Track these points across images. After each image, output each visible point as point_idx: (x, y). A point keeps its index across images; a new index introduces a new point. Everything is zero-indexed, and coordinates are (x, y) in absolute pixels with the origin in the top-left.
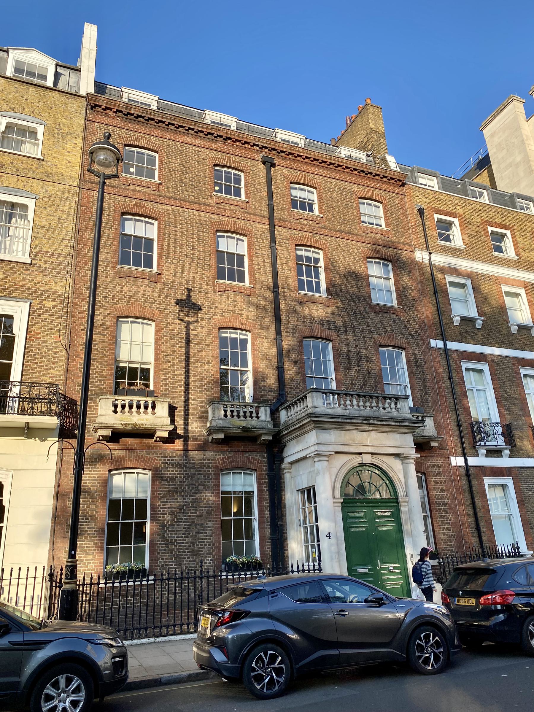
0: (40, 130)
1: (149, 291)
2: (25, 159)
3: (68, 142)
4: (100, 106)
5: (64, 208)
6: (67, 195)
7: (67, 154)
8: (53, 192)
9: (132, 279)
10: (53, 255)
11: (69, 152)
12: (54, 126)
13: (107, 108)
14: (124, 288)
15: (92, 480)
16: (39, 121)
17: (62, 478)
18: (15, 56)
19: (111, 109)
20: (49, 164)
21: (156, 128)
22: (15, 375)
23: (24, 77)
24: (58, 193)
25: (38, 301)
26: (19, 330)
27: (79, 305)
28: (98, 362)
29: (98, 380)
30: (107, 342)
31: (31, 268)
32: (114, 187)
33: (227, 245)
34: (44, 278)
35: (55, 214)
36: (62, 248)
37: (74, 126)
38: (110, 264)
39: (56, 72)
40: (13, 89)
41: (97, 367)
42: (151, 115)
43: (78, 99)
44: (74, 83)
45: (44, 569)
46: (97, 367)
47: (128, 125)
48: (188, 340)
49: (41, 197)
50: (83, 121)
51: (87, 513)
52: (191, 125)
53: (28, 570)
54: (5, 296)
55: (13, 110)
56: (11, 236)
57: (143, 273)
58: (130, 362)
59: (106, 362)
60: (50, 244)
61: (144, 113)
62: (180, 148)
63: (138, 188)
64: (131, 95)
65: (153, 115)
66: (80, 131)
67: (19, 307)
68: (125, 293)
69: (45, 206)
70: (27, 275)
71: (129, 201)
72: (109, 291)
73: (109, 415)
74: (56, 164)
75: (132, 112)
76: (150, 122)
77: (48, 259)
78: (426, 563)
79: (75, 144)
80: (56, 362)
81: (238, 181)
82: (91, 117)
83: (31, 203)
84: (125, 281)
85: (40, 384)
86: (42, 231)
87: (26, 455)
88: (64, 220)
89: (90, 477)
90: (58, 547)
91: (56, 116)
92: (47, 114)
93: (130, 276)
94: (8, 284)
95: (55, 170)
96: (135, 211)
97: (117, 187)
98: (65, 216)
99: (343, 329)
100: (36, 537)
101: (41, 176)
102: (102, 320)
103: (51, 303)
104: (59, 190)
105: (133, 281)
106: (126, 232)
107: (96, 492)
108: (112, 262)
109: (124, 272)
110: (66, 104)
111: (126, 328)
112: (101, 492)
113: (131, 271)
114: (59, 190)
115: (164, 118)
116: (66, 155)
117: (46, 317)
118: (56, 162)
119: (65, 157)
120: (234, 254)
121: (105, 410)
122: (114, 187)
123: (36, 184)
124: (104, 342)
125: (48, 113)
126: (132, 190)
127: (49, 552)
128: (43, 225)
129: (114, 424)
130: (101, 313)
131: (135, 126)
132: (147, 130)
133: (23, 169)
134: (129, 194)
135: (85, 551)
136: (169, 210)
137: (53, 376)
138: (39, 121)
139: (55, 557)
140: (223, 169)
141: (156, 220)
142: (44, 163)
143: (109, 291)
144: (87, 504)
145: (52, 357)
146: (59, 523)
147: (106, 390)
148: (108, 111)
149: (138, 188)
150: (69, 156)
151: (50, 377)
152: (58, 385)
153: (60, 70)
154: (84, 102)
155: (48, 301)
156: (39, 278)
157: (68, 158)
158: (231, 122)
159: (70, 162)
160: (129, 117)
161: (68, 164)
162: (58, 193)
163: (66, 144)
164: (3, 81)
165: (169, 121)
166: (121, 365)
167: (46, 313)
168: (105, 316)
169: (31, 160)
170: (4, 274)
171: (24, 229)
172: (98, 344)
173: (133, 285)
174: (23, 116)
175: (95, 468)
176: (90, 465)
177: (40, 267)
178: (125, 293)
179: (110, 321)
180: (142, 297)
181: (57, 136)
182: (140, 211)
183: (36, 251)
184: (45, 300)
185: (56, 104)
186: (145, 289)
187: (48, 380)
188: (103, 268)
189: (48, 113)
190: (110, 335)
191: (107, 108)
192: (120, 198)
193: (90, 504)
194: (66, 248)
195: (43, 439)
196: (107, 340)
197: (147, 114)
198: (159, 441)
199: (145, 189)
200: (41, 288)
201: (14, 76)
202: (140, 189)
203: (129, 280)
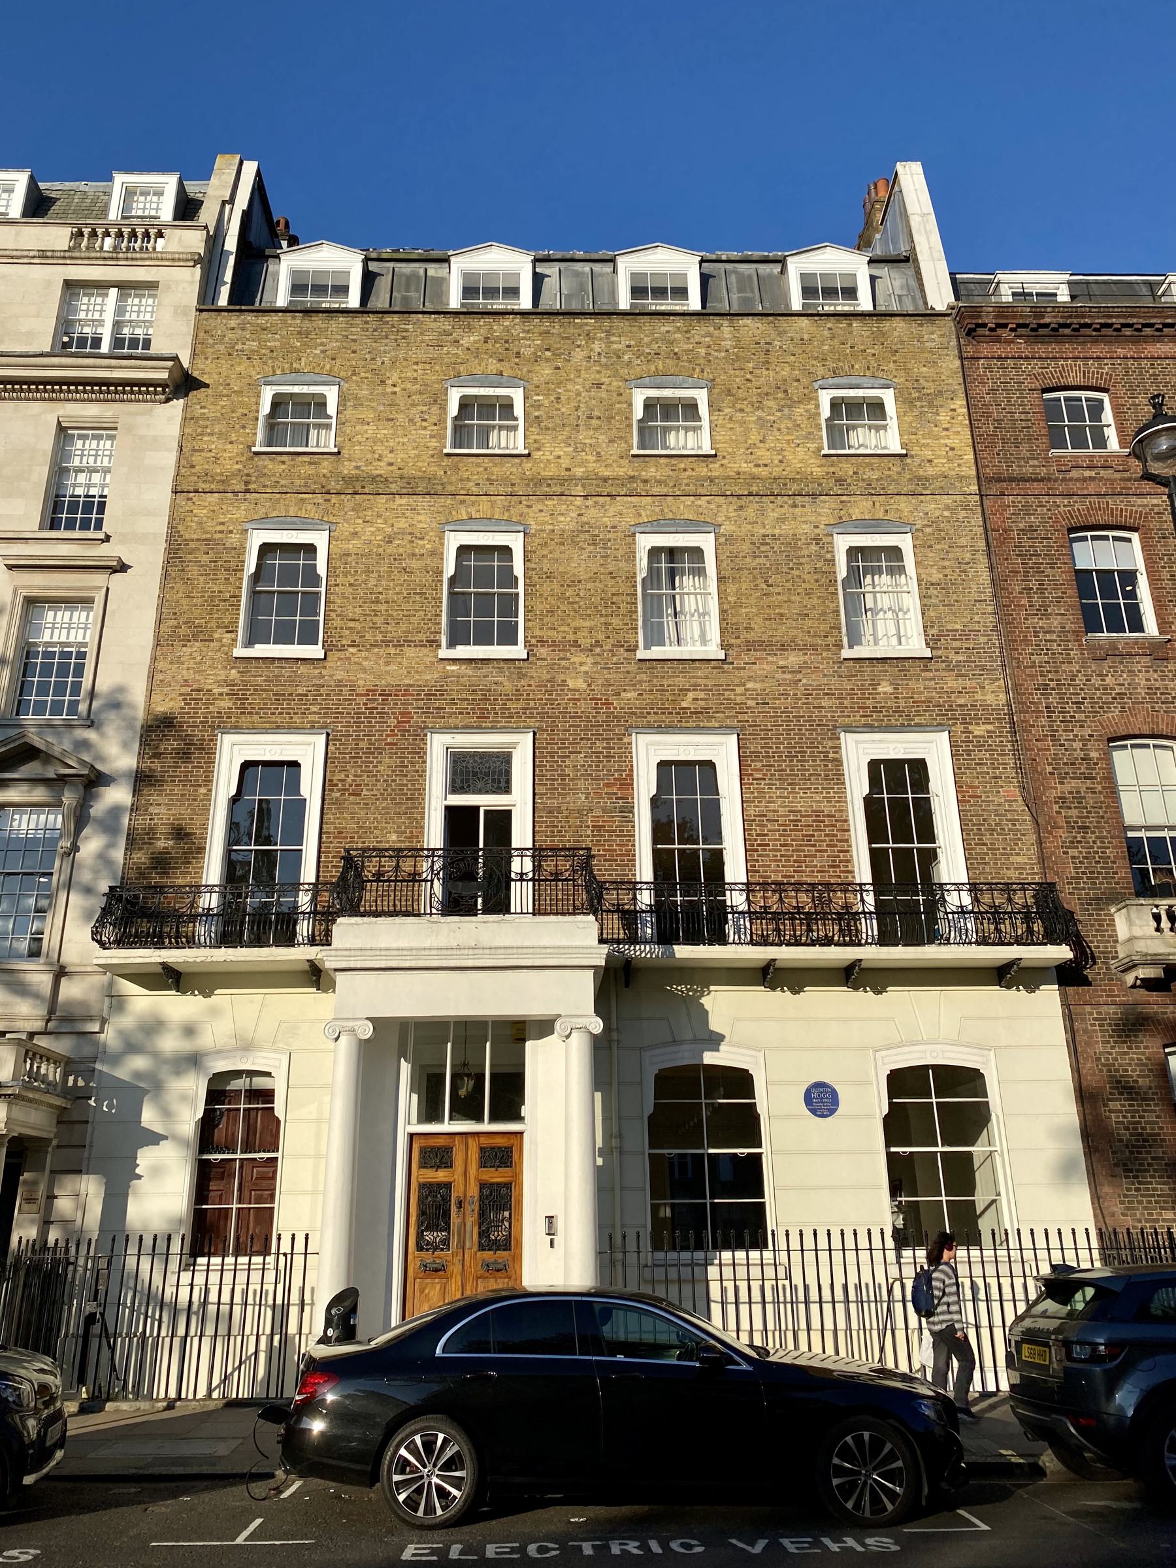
0: (888, 398)
1: (1156, 680)
2: (875, 460)
3: (940, 410)
4: (984, 325)
5: (963, 541)
6: (962, 514)
7: (945, 433)
8: (937, 513)
9: (1118, 659)
10: (965, 635)
11: (947, 429)
12: (909, 385)
13: (999, 326)
14: (1108, 679)
15: (1136, 1065)
16: (882, 381)
17: (1081, 1060)
18: (629, 265)
19: (1005, 326)
20: (917, 460)
21: (1095, 340)
22: (735, 870)
23: (309, 300)
24: (946, 514)
26: (311, 786)
27: (1033, 726)
28: (1093, 832)
29: (1102, 868)
30: (1100, 793)
31: (932, 666)
32: (1042, 480)
33: (1093, 555)
34: (960, 681)
35: (951, 555)
36: (976, 618)
37: (943, 377)
38: (1070, 637)
39: (535, 274)
40: (826, 333)
41: (1094, 842)
42: (1084, 317)
43: (939, 321)
44: (902, 288)
45: (183, 1239)
46: (1094, 842)
47: (1041, 349)
49: (918, 527)
50: (958, 363)
51: (1142, 1128)
52: (1168, 317)
53: (113, 1240)
54: (903, 725)
55: (834, 373)
56: (871, 609)
57: (1136, 643)
58: (1148, 828)
59: (1109, 832)
60: (954, 614)
61: (1070, 317)
62: (1151, 371)
63: (1087, 473)
64: (1010, 283)
65: (1090, 316)
66: (956, 383)
67: (309, 744)
68: (1112, 689)
69: (929, 543)
70: (930, 680)
71: (1078, 505)
72: (1082, 689)
73: (1152, 938)
74: (929, 458)
75: (1047, 320)
76: (1083, 331)
77: (957, 644)
78: (941, 1267)
79: (954, 410)
80: (1019, 839)
81: (1096, 409)
82: (970, 350)
83: (905, 542)
84: (1105, 665)
85: (798, 886)
86: (935, 592)
87: (1008, 1018)
88: (968, 563)
89: (1132, 1059)
90: (1107, 1194)
91: (909, 366)
92: (892, 365)
93: (1113, 652)
94: (902, 703)
95: (930, 471)
96: (1092, 521)
97: (1049, 480)
98: (968, 556)
100: (1065, 1171)
101: (912, 487)
102: (1081, 750)
103: (984, 727)
104: (947, 508)
105: (1122, 663)
106: (1080, 566)
107: (1150, 1088)
108: (1074, 632)
109: (1100, 647)
110: (920, 338)
111: (1122, 759)
112: (1159, 1087)
113: (1113, 644)
114: (947, 508)
115: (1112, 317)
116: (942, 438)
117: (981, 755)
118: (928, 453)
119: (942, 441)
120: (1091, 571)
121: (1140, 927)
122: (1042, 480)
123: (904, 505)
124: (1095, 793)
125: (895, 362)
126: (1077, 480)
127: (1093, 1203)
128: (934, 581)
129: (1169, 954)
130: (1076, 736)
131: (1053, 348)
132: (1079, 350)
133: (877, 480)
134: (1075, 487)
135: (1156, 1202)
136: (1158, 505)
137: (1020, 868)
138: (882, 381)
139: (1105, 1213)
140: (1062, 395)
141: (1135, 529)
142: (909, 461)
143: (1082, 689)
144: (1138, 1111)
145: (1010, 830)
146: (1097, 1150)
147: (1122, 888)
148: (1000, 331)
149: (1087, 473)
150: (948, 437)
151: (1016, 869)
153: (373, 267)
154: (949, 324)
155: (978, 724)
156: (952, 683)
157: (947, 441)
158: (1055, 284)
160: (1042, 331)
161: (950, 453)
162: (946, 514)
163: (938, 415)
164: (902, 324)
165: (1122, 321)
166: (1130, 834)
167: (980, 747)
168: (1084, 742)
169: (886, 459)
170: (891, 684)
171: (696, 594)
172: (1084, 798)
173: (1122, 671)
174: (853, 380)
175: (1137, 1042)
176: (1127, 1036)
177: (947, 661)
178: (1112, 689)
179: (1097, 750)
180: (1147, 693)
181: (918, 404)
182: (1103, 519)
183: (935, 631)
184: (971, 724)
185: (902, 342)
186: (1147, 675)
188: (1059, 645)
189: (895, 362)
190: (1104, 778)
191: (999, 326)
192: (1058, 500)
193: (1144, 1111)
194: (985, 617)
195: (1031, 988)
196: (1099, 788)
197: (1076, 317)
198: (1140, 987)
199: (1102, 472)
200: (961, 701)
201: (463, 305)
202: (1093, 474)
203: (1113, 662)
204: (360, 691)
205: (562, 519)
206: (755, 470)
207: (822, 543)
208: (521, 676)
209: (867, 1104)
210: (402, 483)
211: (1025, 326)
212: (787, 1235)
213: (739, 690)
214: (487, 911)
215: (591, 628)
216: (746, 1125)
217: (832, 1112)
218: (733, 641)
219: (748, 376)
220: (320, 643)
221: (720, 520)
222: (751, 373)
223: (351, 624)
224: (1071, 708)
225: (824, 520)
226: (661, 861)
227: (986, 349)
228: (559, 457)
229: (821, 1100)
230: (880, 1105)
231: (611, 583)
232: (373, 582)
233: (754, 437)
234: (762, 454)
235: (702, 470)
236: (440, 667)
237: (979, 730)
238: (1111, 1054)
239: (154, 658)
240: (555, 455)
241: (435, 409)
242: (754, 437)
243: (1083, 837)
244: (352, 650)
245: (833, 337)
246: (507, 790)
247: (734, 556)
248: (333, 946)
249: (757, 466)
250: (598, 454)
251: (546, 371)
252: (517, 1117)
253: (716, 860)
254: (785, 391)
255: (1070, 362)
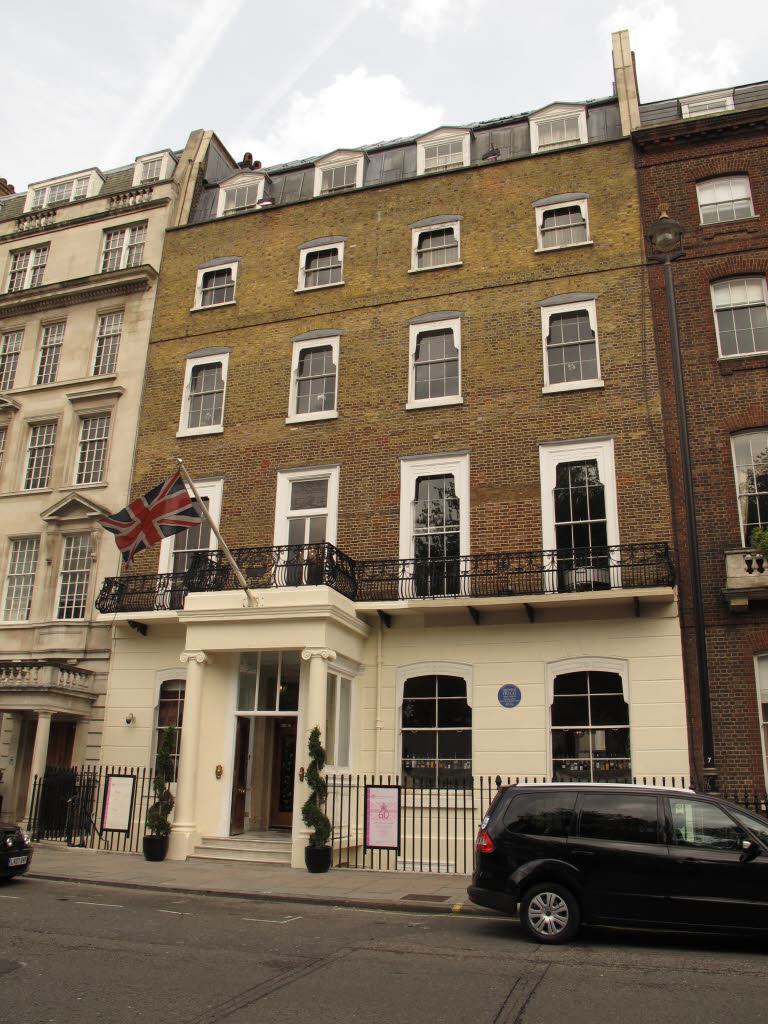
11: (624, 221)
25: (622, 435)
26: (462, 491)
28: (714, 503)
41: (715, 509)
46: (715, 509)
48: (529, 282)
71: (717, 261)
79: (630, 207)
85: (643, 547)
99: (127, 195)
126: (719, 243)
128: (610, 331)
134: (716, 250)
150: (625, 227)
152: (666, 543)
154: (626, 147)
157: (624, 230)
159: (628, 234)
165: (755, 120)
168: (713, 436)
179: (722, 442)
184: (630, 431)
187: (652, 537)
191: (663, 140)
199: (739, 235)
200: (624, 416)
204: (243, 450)
205: (363, 323)
206: (490, 271)
207: (534, 315)
208: (335, 429)
209: (539, 698)
210: (271, 315)
211: (683, 137)
212: (481, 780)
213: (473, 423)
214: (310, 583)
215: (379, 392)
216: (463, 714)
217: (515, 704)
218: (469, 390)
219: (488, 207)
220: (336, 407)
221: (464, 308)
222: (490, 204)
223: (239, 409)
224: (704, 412)
225: (535, 298)
226: (562, 533)
227: (654, 159)
228: (364, 283)
229: (510, 696)
230: (548, 696)
231: (393, 360)
232: (252, 380)
233: (490, 248)
234: (496, 258)
235: (455, 276)
236: (287, 428)
237: (635, 436)
238: (714, 660)
239: (138, 443)
240: (363, 280)
241: (292, 265)
242: (490, 248)
243: (707, 507)
244: (239, 425)
245: (546, 170)
246: (325, 506)
247: (472, 332)
248: (185, 609)
249: (491, 267)
250: (389, 276)
251: (359, 227)
252: (295, 708)
253: (600, 530)
254: (512, 213)
255: (718, 157)
